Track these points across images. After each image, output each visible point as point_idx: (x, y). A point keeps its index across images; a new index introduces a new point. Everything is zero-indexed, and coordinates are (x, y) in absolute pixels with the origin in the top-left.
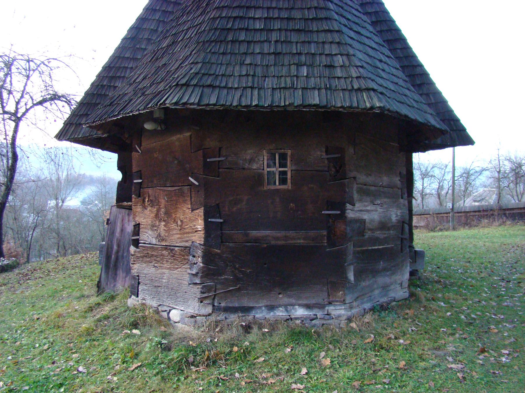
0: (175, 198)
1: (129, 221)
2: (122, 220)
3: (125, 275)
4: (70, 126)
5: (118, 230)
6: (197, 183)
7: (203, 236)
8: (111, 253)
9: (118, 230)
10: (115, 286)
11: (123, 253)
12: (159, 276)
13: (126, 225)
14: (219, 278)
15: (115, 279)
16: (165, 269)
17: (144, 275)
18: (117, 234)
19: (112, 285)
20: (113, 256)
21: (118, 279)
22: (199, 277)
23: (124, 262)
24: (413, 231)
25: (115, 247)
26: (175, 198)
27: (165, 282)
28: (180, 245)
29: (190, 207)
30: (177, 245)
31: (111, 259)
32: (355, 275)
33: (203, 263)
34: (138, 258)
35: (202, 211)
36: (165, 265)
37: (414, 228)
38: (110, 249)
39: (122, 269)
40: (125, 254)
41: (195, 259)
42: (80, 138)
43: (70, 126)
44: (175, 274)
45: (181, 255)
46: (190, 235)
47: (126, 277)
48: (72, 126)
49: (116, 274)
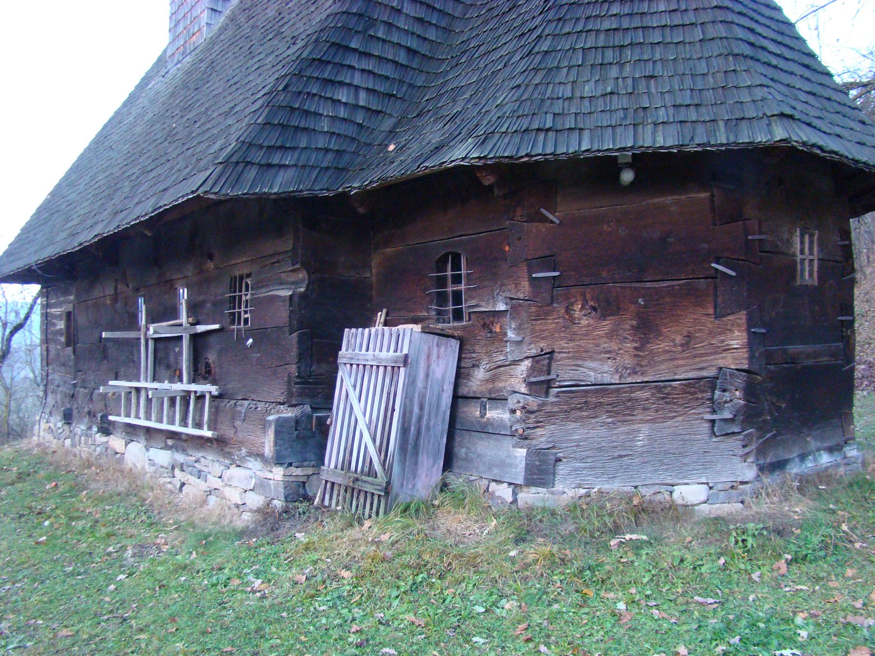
0: (669, 300)
1: (438, 357)
2: (428, 356)
3: (431, 461)
4: (245, 167)
5: (421, 375)
6: (733, 273)
7: (746, 355)
8: (410, 422)
9: (421, 375)
10: (414, 486)
11: (429, 419)
12: (622, 437)
13: (433, 366)
14: (755, 420)
15: (415, 475)
16: (639, 423)
17: (575, 444)
18: (420, 384)
19: (410, 486)
20: (413, 428)
21: (419, 472)
22: (737, 422)
23: (430, 437)
24: (199, 331)
25: (416, 410)
26: (669, 300)
27: (642, 447)
28: (686, 377)
29: (711, 311)
30: (677, 377)
31: (409, 433)
32: (410, 430)
33: (745, 399)
34: (551, 415)
35: (744, 317)
36: (640, 417)
37: (64, 331)
38: (408, 414)
39: (427, 453)
40: (432, 423)
41: (727, 394)
42: (275, 194)
43: (245, 167)
44: (669, 428)
45: (686, 393)
46: (709, 358)
47: (433, 466)
48: (249, 167)
49: (416, 463)
